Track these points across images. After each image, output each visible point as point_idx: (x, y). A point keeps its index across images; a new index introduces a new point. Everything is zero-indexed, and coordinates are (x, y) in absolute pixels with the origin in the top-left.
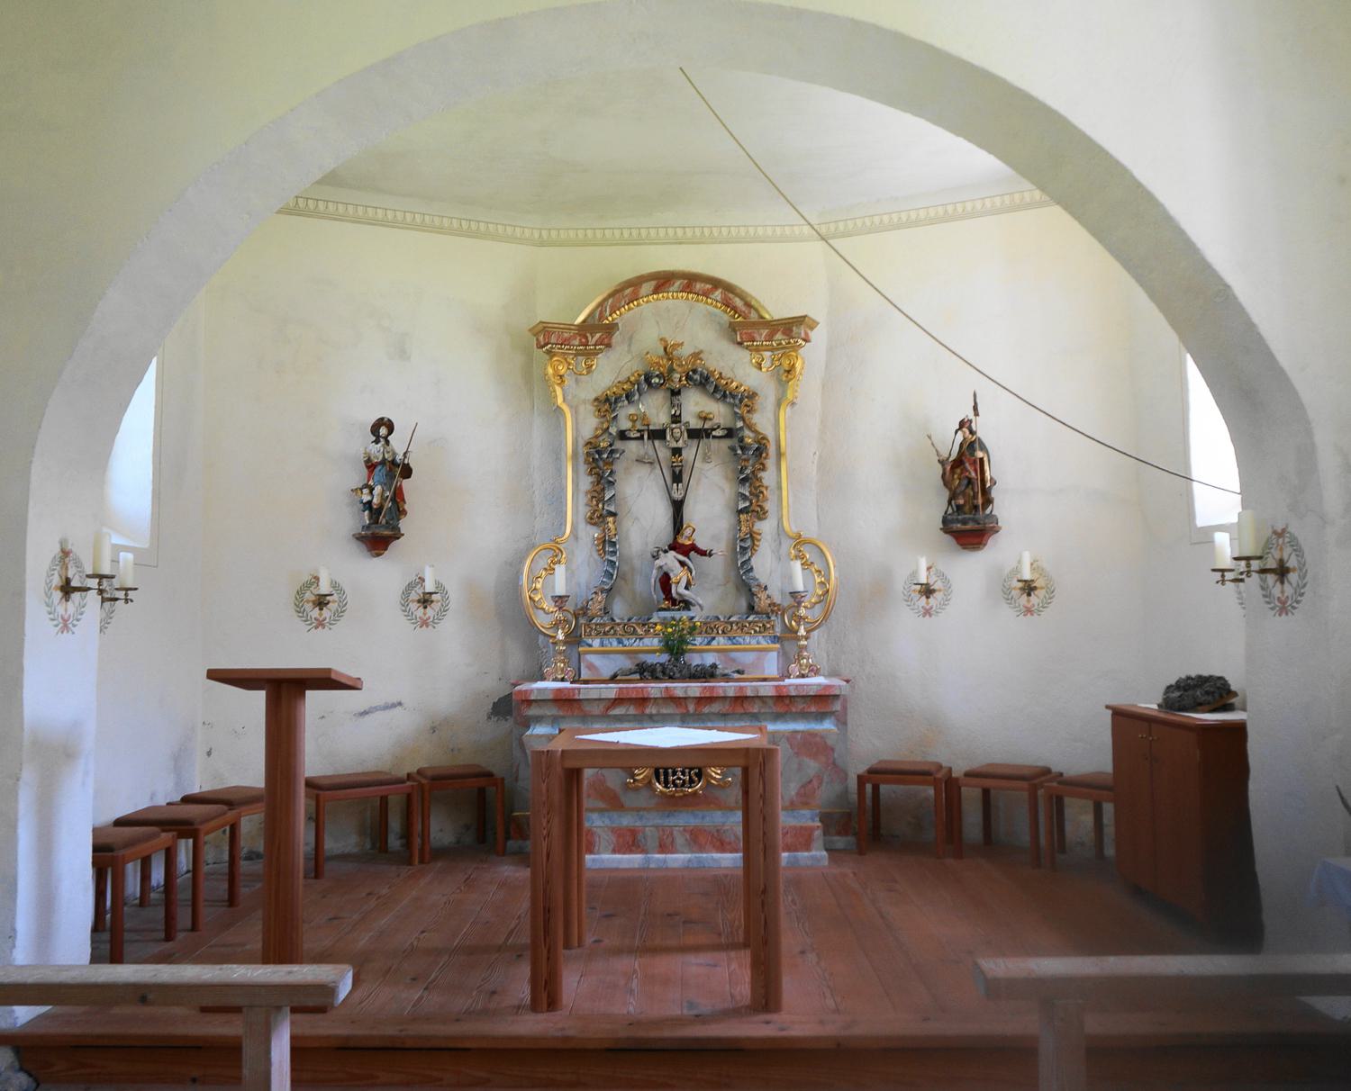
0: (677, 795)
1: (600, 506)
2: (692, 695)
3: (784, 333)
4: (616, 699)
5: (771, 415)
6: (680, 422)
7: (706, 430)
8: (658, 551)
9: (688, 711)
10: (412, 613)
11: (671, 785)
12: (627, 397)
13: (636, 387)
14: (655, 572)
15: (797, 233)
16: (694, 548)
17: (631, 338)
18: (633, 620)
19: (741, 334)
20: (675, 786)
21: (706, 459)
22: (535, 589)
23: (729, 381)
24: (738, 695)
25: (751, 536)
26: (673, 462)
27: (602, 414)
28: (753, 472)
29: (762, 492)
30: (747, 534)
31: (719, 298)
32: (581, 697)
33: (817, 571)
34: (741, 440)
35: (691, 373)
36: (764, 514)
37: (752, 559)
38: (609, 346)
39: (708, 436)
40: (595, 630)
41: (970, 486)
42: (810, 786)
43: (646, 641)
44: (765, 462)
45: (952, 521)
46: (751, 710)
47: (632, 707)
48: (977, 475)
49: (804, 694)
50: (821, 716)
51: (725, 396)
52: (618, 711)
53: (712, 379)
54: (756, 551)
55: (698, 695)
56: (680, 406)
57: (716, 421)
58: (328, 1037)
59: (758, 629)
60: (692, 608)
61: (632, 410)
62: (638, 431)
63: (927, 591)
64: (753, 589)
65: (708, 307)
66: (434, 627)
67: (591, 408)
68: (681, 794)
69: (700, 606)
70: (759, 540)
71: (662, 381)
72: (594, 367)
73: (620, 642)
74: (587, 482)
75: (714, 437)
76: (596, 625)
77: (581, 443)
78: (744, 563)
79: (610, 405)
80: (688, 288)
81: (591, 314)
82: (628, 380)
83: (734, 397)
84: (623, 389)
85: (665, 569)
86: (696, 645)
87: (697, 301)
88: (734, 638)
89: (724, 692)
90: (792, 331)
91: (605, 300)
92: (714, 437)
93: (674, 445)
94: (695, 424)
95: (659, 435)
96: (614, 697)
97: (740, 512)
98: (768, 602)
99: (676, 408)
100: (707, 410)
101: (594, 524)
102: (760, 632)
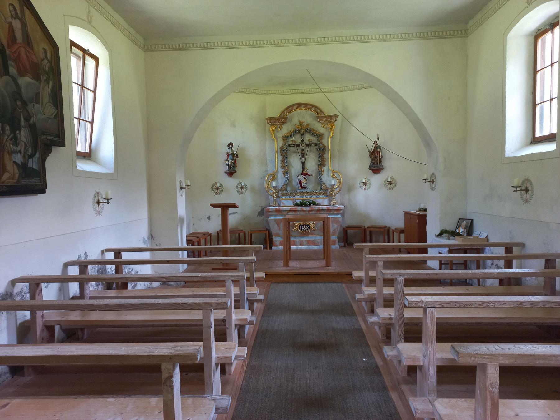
4: (290, 210)
7: (310, 144)
16: (307, 174)
20: (304, 230)
21: (310, 151)
27: (284, 140)
38: (286, 123)
39: (311, 146)
50: (338, 214)
56: (304, 138)
57: (313, 142)
62: (293, 145)
63: (365, 184)
67: (281, 139)
74: (280, 158)
77: (279, 148)
85: (300, 179)
92: (312, 146)
93: (302, 148)
94: (308, 142)
95: (298, 145)
97: (319, 165)
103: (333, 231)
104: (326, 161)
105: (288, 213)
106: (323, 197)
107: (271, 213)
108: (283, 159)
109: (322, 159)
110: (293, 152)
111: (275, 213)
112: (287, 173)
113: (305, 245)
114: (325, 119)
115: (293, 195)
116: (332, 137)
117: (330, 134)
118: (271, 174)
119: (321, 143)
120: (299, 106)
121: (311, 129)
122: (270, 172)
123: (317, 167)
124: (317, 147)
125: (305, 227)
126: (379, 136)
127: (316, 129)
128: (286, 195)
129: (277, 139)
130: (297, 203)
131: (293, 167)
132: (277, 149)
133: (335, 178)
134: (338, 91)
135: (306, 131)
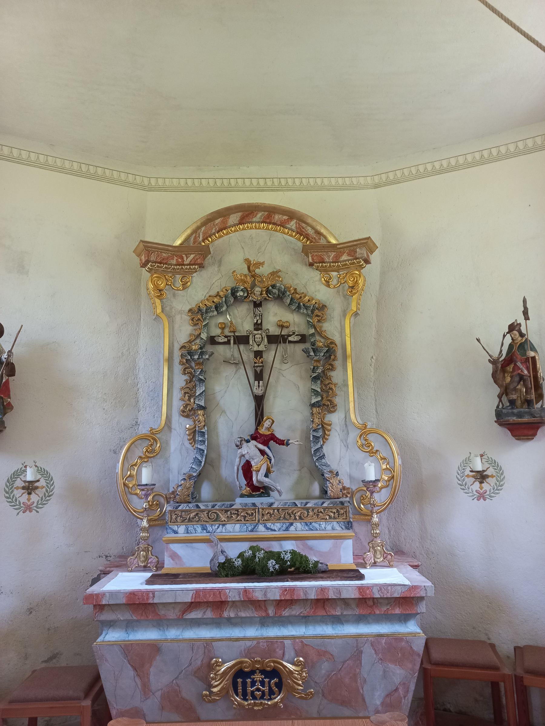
0: (256, 708)
1: (192, 400)
2: (272, 598)
3: (349, 255)
4: (192, 603)
5: (337, 324)
6: (261, 329)
7: (283, 336)
8: (241, 441)
9: (268, 614)
10: (16, 500)
11: (249, 697)
12: (216, 308)
13: (224, 299)
14: (238, 460)
15: (355, 183)
16: (273, 437)
17: (220, 262)
18: (217, 507)
19: (312, 256)
20: (254, 697)
21: (284, 360)
22: (130, 476)
23: (302, 295)
24: (319, 597)
25: (322, 426)
26: (255, 363)
27: (195, 322)
28: (323, 372)
29: (331, 389)
30: (319, 425)
31: (293, 227)
32: (156, 601)
33: (382, 459)
34: (313, 344)
35: (270, 288)
36: (333, 407)
37: (324, 447)
38: (201, 266)
39: (285, 342)
40: (181, 516)
41: (522, 383)
42: (396, 694)
43: (229, 527)
44: (333, 363)
45: (507, 415)
46: (333, 613)
47: (209, 609)
48: (529, 372)
49: (389, 595)
50: (404, 619)
51: (299, 307)
52: (194, 615)
53: (288, 293)
54: (327, 439)
55: (278, 598)
56: (261, 316)
57: (292, 329)
58: (128, 590)
59: (332, 514)
60: (271, 493)
61: (221, 320)
62: (226, 337)
63: (481, 477)
64: (326, 475)
65: (285, 236)
66: (38, 512)
67: (187, 318)
68: (260, 708)
69: (278, 491)
70: (329, 430)
71: (246, 295)
72: (189, 284)
73: (204, 528)
74: (180, 380)
75: (290, 342)
76: (182, 511)
77: (177, 347)
78: (317, 451)
79: (202, 315)
80: (267, 220)
81: (187, 240)
82: (218, 295)
83: (306, 308)
84: (213, 302)
85: (247, 457)
86: (275, 530)
87: (276, 231)
88: (311, 523)
89: (306, 593)
90: (356, 252)
91: (199, 228)
92: (290, 342)
93: (256, 348)
94: (274, 331)
95: (242, 340)
96: (190, 601)
97: (313, 405)
98: (340, 487)
99: (258, 318)
100: (284, 319)
101: (187, 416)
102: (334, 518)
103: (389, 695)
104: (338, 392)
105: (184, 612)
106: (333, 529)
107: (106, 616)
108: (190, 385)
109: (326, 385)
110: (226, 362)
111: (127, 616)
112: (203, 434)
113: (277, 590)
114: (332, 255)
115: (217, 519)
116: (356, 314)
117: (349, 304)
118: (143, 438)
119: (320, 334)
120: (247, 216)
121: (287, 288)
122: (143, 430)
123: (309, 414)
124: (308, 345)
125: (263, 683)
126: (528, 306)
127: (300, 289)
128: (190, 520)
129: (171, 319)
130: (228, 561)
131: (224, 412)
132: (171, 353)
133: (372, 453)
134: (366, 187)
135: (268, 291)
